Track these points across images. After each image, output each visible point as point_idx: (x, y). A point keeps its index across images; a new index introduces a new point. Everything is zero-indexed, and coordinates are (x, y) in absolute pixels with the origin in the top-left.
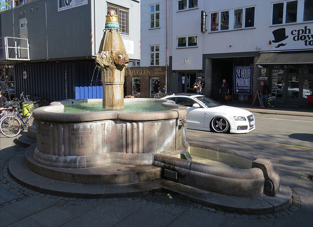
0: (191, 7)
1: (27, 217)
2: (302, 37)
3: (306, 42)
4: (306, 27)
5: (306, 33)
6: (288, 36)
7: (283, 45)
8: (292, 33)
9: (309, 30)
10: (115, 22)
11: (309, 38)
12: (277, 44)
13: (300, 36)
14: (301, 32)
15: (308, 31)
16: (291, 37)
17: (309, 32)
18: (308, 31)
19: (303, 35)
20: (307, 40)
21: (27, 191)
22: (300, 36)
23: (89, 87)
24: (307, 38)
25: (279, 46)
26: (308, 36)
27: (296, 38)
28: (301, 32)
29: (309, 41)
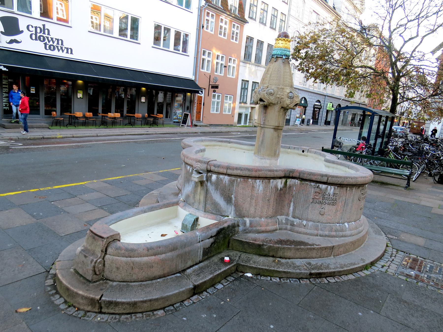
0: (39, 108)
1: (297, 182)
2: (40, 36)
3: (46, 44)
4: (44, 26)
5: (44, 33)
6: (22, 32)
7: (16, 41)
8: (28, 27)
9: (62, 41)
10: (166, 31)
11: (49, 42)
12: (9, 38)
13: (38, 35)
14: (38, 30)
15: (46, 31)
16: (26, 34)
17: (62, 44)
18: (46, 31)
19: (41, 34)
20: (46, 42)
21: (96, 237)
22: (38, 35)
23: (401, 80)
24: (46, 41)
25: (11, 42)
26: (48, 38)
27: (34, 37)
28: (38, 30)
29: (49, 44)
